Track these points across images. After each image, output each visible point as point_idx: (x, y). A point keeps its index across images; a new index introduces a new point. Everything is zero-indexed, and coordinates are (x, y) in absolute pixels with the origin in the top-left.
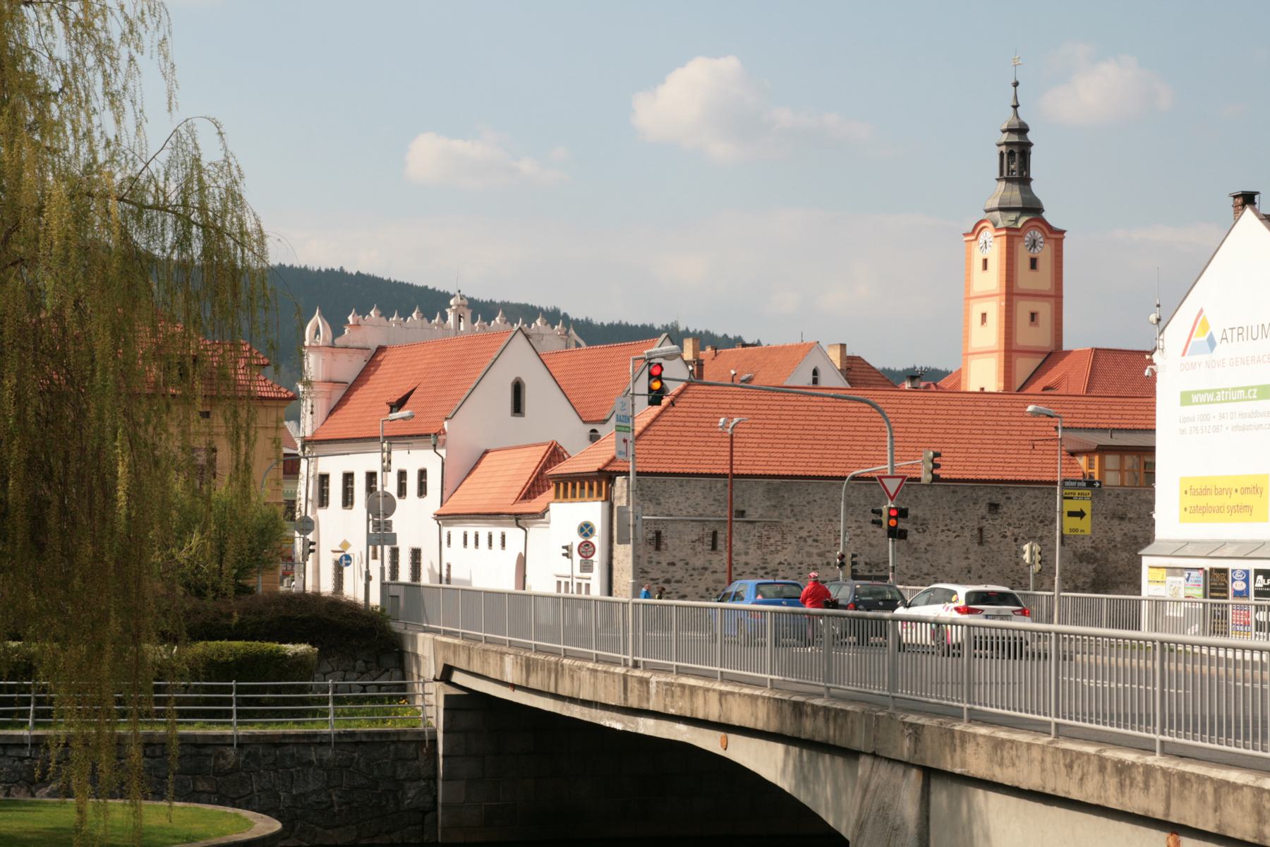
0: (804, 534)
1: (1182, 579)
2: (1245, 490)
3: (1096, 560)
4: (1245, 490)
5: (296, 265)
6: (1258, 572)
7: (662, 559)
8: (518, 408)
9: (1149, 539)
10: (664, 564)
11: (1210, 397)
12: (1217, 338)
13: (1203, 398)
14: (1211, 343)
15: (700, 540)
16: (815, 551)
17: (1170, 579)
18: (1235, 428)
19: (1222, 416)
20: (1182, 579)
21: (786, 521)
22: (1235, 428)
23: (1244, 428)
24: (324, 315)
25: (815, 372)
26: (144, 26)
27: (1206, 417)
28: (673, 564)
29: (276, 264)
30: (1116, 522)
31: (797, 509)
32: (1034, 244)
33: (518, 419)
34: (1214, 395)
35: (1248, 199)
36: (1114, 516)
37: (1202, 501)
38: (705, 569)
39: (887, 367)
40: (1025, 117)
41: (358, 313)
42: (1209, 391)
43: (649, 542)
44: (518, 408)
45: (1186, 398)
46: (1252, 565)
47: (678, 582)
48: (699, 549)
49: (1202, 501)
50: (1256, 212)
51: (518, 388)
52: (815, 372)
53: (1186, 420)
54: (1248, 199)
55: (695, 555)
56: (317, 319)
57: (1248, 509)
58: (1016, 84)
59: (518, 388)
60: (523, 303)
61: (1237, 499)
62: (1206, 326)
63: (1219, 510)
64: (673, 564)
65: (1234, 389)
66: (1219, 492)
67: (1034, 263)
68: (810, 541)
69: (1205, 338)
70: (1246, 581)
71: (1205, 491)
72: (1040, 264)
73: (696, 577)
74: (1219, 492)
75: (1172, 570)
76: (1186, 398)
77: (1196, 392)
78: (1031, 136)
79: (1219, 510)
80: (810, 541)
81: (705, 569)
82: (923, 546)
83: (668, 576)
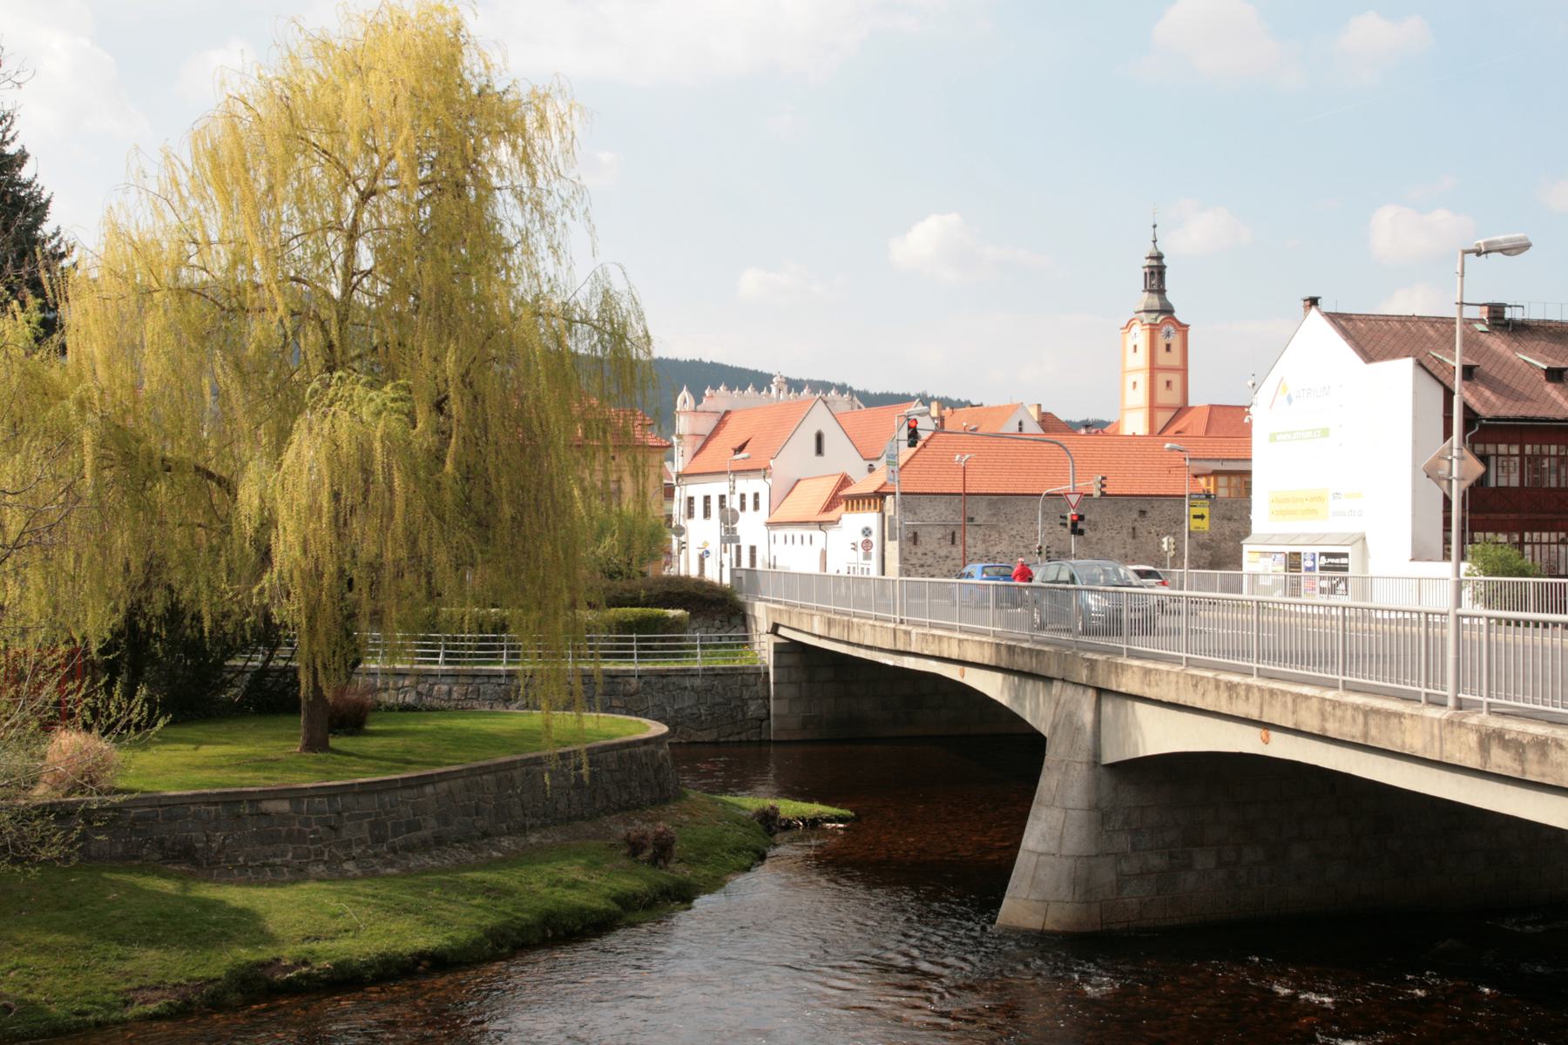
0: (1014, 533)
2: (1312, 499)
3: (1212, 548)
4: (1312, 499)
6: (1321, 554)
8: (819, 451)
10: (920, 554)
12: (1293, 397)
15: (944, 538)
21: (1001, 524)
25: (1020, 424)
28: (925, 554)
30: (1225, 522)
31: (1009, 516)
32: (1168, 334)
33: (820, 458)
35: (1314, 302)
36: (1224, 518)
38: (947, 557)
40: (1161, 248)
42: (1289, 433)
44: (819, 451)
46: (1318, 550)
47: (929, 566)
50: (1319, 310)
54: (1314, 302)
57: (1314, 512)
58: (1155, 226)
64: (925, 554)
67: (1168, 348)
68: (1018, 537)
70: (1314, 560)
72: (1173, 348)
78: (1165, 261)
80: (1018, 537)
81: (947, 557)
82: (1094, 540)
83: (922, 562)
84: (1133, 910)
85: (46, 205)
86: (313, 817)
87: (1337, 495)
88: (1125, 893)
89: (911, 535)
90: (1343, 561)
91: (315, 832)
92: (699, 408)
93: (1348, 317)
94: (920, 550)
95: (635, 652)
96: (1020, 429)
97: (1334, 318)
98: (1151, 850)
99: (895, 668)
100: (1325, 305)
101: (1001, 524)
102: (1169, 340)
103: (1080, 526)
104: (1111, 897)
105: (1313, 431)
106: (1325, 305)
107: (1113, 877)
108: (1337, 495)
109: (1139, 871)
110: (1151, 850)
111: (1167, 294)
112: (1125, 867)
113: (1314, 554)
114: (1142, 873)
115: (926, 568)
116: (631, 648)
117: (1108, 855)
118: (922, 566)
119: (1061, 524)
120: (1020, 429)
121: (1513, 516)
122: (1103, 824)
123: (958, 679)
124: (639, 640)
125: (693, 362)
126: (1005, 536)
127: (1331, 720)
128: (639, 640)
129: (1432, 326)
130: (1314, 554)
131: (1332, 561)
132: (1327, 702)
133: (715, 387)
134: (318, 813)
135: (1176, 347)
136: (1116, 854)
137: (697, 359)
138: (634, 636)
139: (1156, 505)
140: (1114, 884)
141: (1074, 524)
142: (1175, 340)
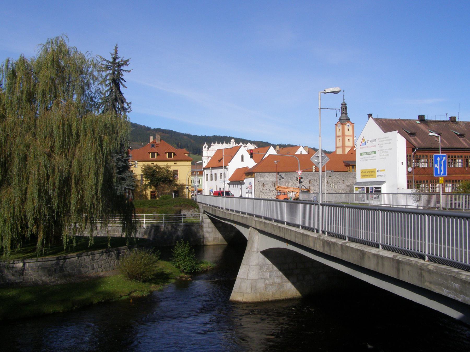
0: (293, 183)
1: (361, 189)
2: (372, 172)
3: (350, 186)
4: (372, 172)
5: (218, 135)
6: (374, 188)
7: (264, 189)
8: (242, 161)
9: (202, 156)
10: (265, 190)
11: (366, 154)
12: (366, 142)
13: (364, 154)
14: (365, 143)
15: (272, 185)
16: (295, 186)
17: (359, 189)
18: (370, 160)
19: (368, 158)
20: (361, 189)
21: (289, 181)
22: (370, 160)
23: (372, 160)
24: (207, 144)
25: (301, 152)
26: (124, 81)
27: (365, 158)
28: (267, 190)
29: (338, 154)
30: (354, 179)
31: (291, 178)
32: (348, 126)
33: (242, 162)
34: (366, 153)
35: (370, 115)
36: (353, 178)
37: (365, 174)
38: (273, 190)
39: (158, 128)
40: (346, 101)
41: (213, 143)
42: (365, 153)
43: (262, 185)
44: (242, 161)
45: (361, 154)
46: (373, 186)
47: (268, 193)
48: (272, 187)
49: (365, 174)
50: (372, 118)
51: (242, 156)
52: (301, 152)
53: (361, 158)
54: (370, 115)
55: (271, 188)
56: (205, 144)
57: (372, 175)
58: (344, 96)
59: (242, 156)
60: (241, 138)
61: (371, 173)
62: (364, 140)
63: (367, 176)
64: (267, 190)
65: (370, 152)
66: (368, 172)
67: (348, 130)
68: (294, 184)
69: (364, 142)
70: (372, 189)
71: (365, 172)
72: (349, 130)
73: (271, 192)
74: (368, 172)
75: (359, 188)
76: (361, 154)
77: (363, 153)
78: (347, 105)
79: (367, 176)
80: (294, 184)
81: (273, 190)
82: (316, 185)
83: (266, 192)
84: (270, 295)
85: (419, 116)
86: (30, 268)
87: (378, 171)
88: (267, 291)
89: (262, 184)
90: (380, 189)
91: (30, 273)
92: (210, 149)
93: (381, 120)
94: (265, 189)
95: (145, 217)
96: (301, 153)
97: (376, 120)
98: (276, 277)
99: (224, 223)
100: (374, 116)
101: (289, 181)
102: (349, 127)
103: (301, 180)
104: (263, 291)
105: (372, 152)
106: (374, 116)
107: (263, 285)
108: (378, 171)
109: (272, 283)
110: (276, 277)
111: (348, 115)
112: (267, 282)
113: (372, 188)
114: (273, 284)
115: (267, 194)
116: (144, 218)
117: (262, 279)
118: (266, 193)
119: (296, 180)
120: (301, 153)
121: (427, 176)
122: (260, 269)
123: (235, 226)
124: (146, 216)
125: (224, 136)
126: (290, 184)
127: (11, 251)
128: (146, 216)
129: (405, 122)
130: (372, 188)
131: (377, 189)
132: (296, 233)
133: (214, 143)
134: (31, 267)
135: (351, 130)
136: (264, 278)
137: (225, 136)
138: (145, 215)
139: (334, 175)
140: (264, 287)
141: (300, 180)
142: (350, 127)
